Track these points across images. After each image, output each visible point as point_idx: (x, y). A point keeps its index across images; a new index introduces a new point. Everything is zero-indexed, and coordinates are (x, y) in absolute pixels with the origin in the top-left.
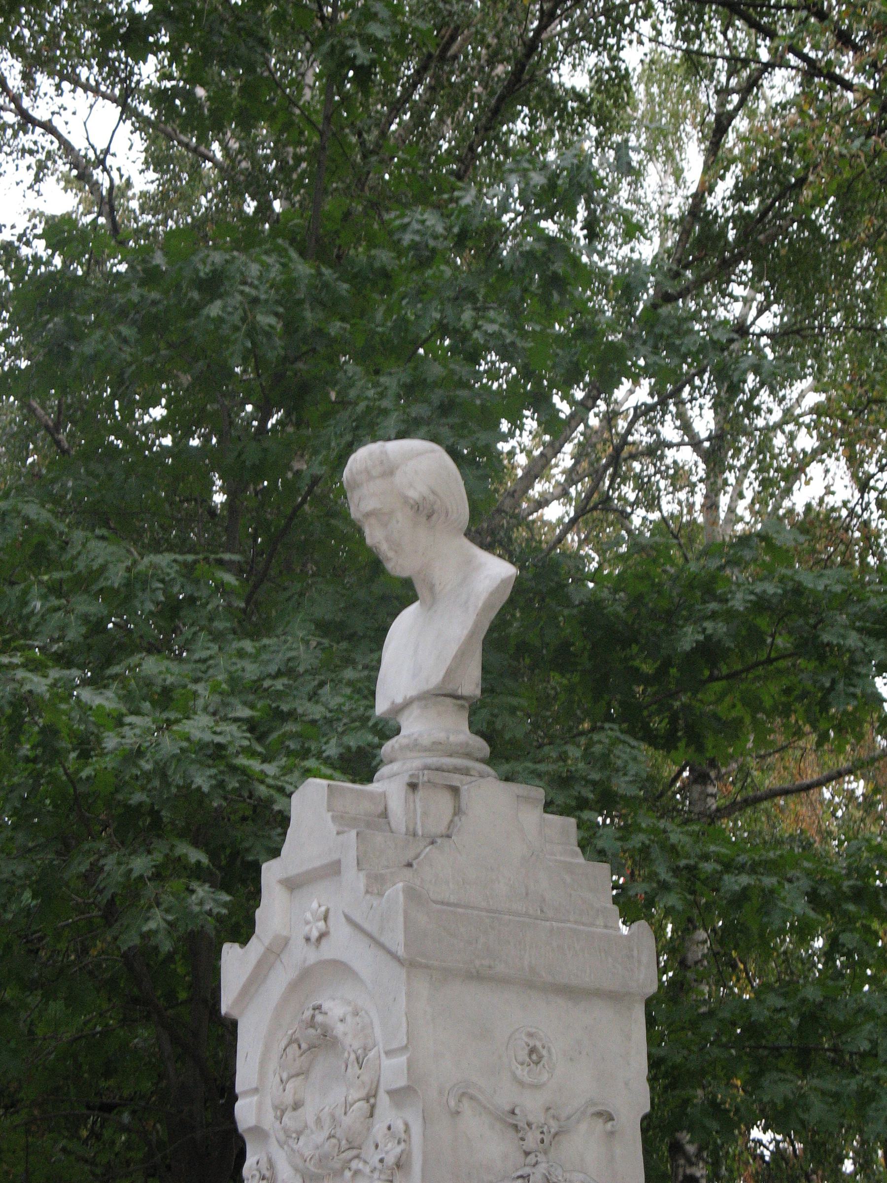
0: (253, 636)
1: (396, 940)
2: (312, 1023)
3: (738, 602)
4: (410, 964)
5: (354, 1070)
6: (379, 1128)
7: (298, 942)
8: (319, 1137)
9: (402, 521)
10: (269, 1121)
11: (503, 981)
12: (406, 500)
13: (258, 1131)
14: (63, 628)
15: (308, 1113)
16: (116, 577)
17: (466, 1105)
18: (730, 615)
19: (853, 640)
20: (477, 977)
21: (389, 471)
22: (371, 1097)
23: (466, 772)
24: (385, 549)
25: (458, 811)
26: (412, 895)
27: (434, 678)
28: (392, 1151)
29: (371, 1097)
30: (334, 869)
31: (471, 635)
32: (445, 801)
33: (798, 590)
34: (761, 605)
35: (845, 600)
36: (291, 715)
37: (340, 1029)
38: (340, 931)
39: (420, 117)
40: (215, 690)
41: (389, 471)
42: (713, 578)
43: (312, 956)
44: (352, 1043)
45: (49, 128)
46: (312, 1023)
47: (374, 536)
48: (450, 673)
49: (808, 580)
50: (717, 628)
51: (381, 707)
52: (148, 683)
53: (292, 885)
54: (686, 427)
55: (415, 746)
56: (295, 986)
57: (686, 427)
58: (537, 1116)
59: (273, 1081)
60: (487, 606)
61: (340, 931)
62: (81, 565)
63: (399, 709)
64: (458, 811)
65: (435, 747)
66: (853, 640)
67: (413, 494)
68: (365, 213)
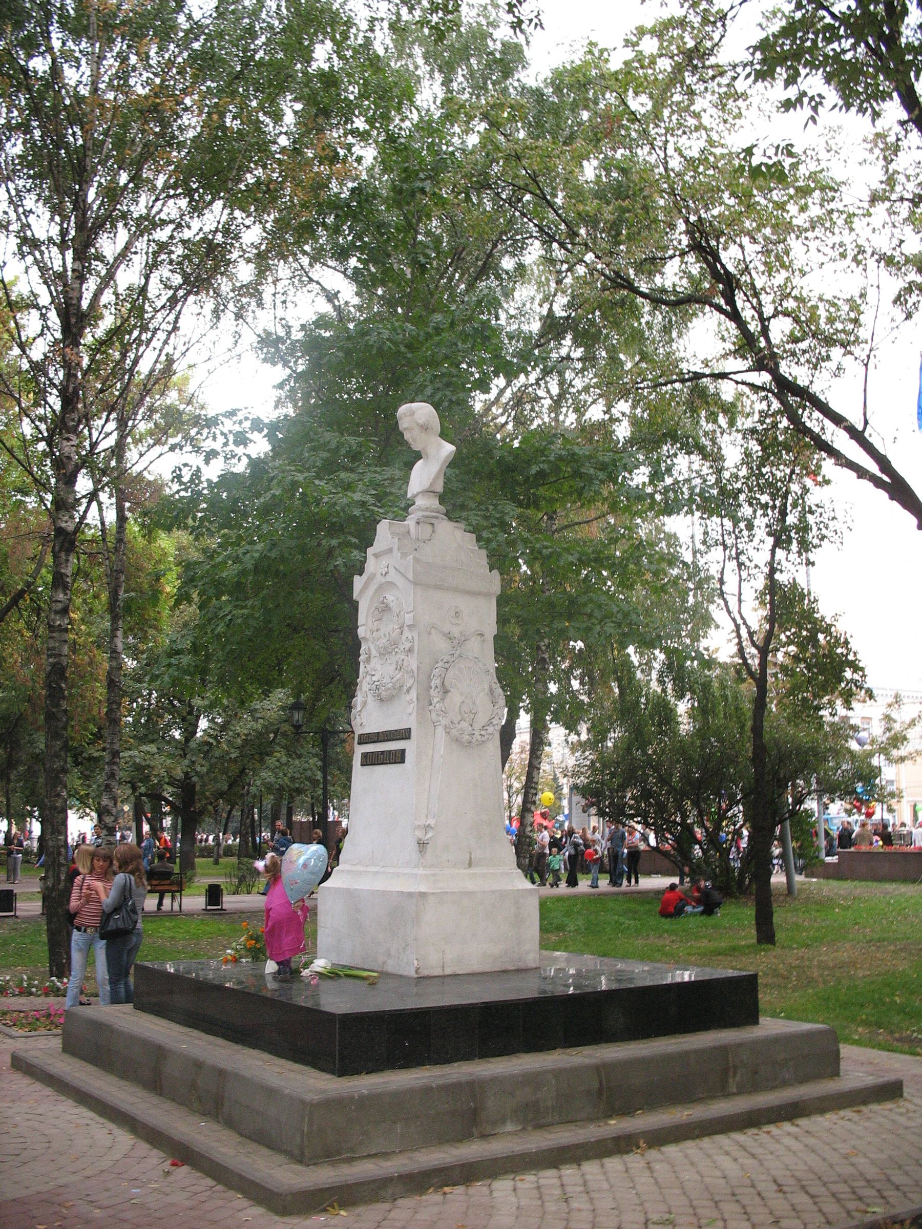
0: (381, 466)
1: (410, 576)
2: (383, 602)
3: (552, 458)
4: (415, 584)
5: (395, 619)
6: (404, 637)
7: (378, 576)
8: (384, 640)
9: (417, 432)
10: (369, 636)
11: (448, 589)
12: (418, 424)
13: (364, 638)
14: (315, 462)
15: (381, 633)
16: (333, 445)
17: (433, 631)
18: (549, 462)
19: (592, 471)
20: (438, 587)
21: (412, 413)
22: (401, 628)
23: (437, 518)
24: (410, 441)
25: (433, 531)
26: (416, 560)
27: (426, 485)
28: (407, 645)
29: (401, 628)
30: (390, 550)
31: (440, 471)
32: (429, 527)
33: (574, 454)
34: (560, 458)
35: (590, 457)
36: (391, 493)
37: (391, 605)
38: (392, 571)
39: (451, 279)
40: (364, 484)
41: (412, 413)
42: (545, 449)
43: (383, 580)
44: (395, 609)
45: (318, 283)
46: (383, 602)
47: (407, 436)
48: (431, 485)
49: (576, 449)
50: (545, 466)
51: (409, 495)
52: (342, 481)
53: (376, 556)
54: (548, 392)
55: (420, 509)
56: (377, 591)
57: (548, 392)
58: (457, 635)
59: (370, 623)
60: (445, 461)
61: (392, 571)
62: (322, 441)
63: (415, 496)
64: (433, 531)
65: (427, 509)
66: (592, 471)
67: (420, 422)
68: (157, 412)
